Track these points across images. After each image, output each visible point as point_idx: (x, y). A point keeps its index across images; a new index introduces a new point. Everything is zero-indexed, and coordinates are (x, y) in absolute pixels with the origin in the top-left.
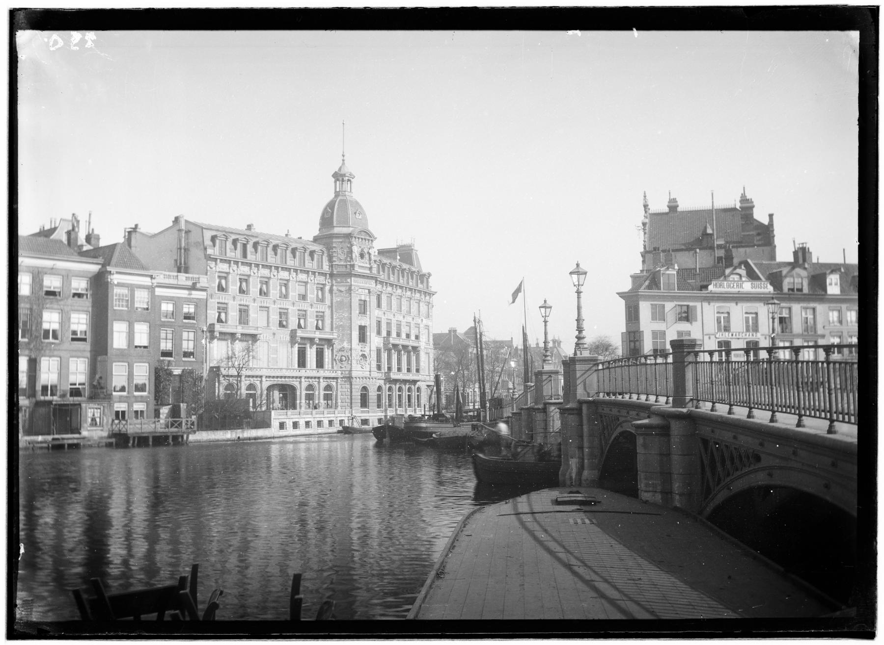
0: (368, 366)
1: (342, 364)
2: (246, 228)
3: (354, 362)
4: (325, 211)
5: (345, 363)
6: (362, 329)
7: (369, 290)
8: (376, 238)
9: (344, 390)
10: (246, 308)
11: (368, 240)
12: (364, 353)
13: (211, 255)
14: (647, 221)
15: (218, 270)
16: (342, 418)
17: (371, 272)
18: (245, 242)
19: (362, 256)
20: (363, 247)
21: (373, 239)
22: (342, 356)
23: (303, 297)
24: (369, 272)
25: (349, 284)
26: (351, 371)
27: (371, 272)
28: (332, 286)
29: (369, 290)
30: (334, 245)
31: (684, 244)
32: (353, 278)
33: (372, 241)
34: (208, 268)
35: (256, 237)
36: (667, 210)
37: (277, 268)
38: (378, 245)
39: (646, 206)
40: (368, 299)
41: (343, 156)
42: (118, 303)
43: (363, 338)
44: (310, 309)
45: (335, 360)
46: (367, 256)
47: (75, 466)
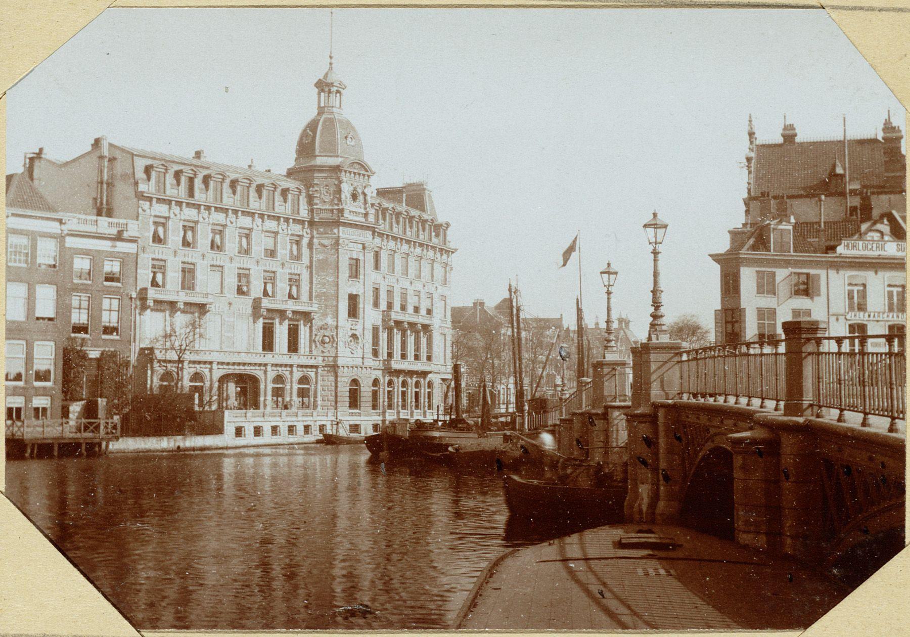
2: (194, 155)
4: (304, 135)
6: (353, 300)
7: (363, 244)
8: (374, 173)
11: (364, 175)
13: (144, 192)
18: (192, 176)
19: (354, 197)
20: (355, 185)
22: (325, 336)
23: (272, 253)
24: (363, 220)
26: (336, 357)
28: (312, 238)
29: (363, 244)
30: (316, 181)
33: (368, 176)
35: (367, 171)
36: (781, 140)
38: (377, 182)
39: (751, 134)
41: (331, 57)
43: (353, 312)
44: (229, 265)
46: (361, 198)
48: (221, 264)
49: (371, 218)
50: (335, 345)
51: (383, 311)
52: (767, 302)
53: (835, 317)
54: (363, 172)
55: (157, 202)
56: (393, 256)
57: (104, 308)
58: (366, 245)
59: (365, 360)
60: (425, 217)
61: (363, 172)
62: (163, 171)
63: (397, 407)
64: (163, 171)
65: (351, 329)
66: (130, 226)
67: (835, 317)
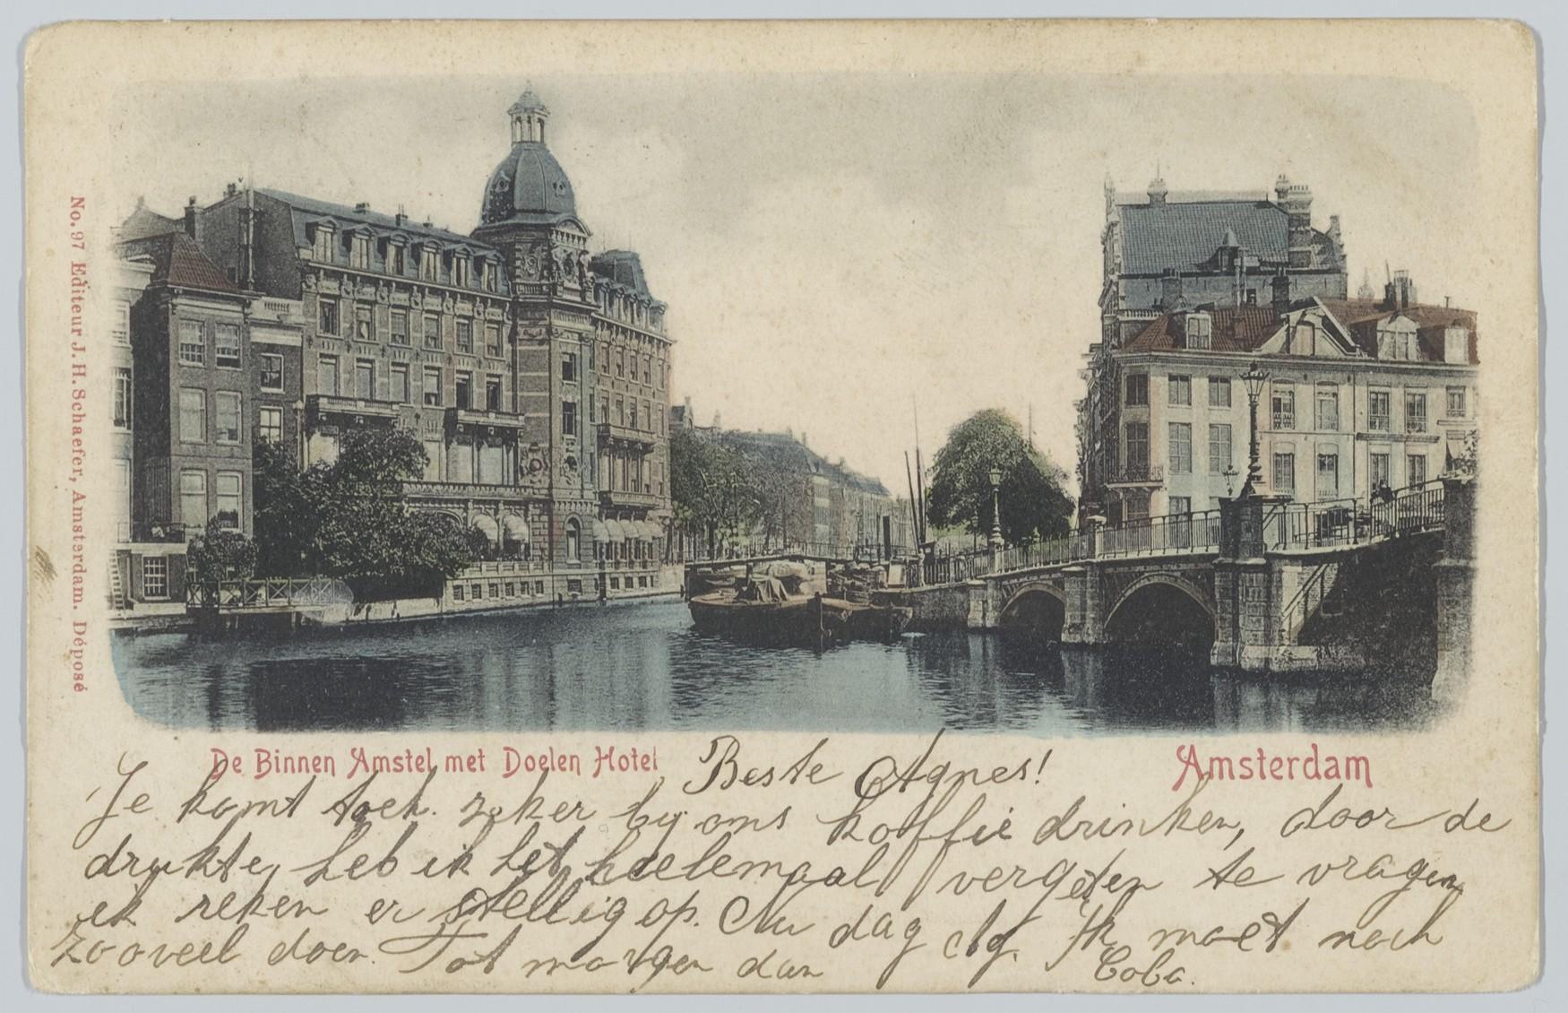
0: (578, 480)
1: (534, 476)
3: (556, 471)
5: (539, 474)
6: (569, 407)
7: (580, 334)
9: (537, 525)
10: (496, 380)
11: (579, 238)
12: (571, 454)
13: (309, 261)
14: (1114, 218)
15: (392, 303)
16: (478, 582)
17: (584, 299)
18: (401, 244)
20: (569, 251)
21: (585, 235)
24: (579, 299)
25: (547, 322)
26: (550, 488)
27: (584, 299)
28: (514, 327)
29: (580, 334)
31: (1198, 266)
32: (553, 311)
33: (585, 240)
34: (304, 285)
35: (581, 230)
37: (388, 284)
40: (577, 353)
42: (185, 352)
43: (569, 426)
44: (477, 369)
45: (521, 468)
46: (576, 270)
47: (1053, 609)
48: (335, 353)
49: (590, 297)
50: (547, 473)
51: (599, 425)
52: (1220, 415)
53: (66, 959)
54: (577, 233)
55: (430, 293)
56: (469, 328)
57: (262, 424)
58: (584, 335)
59: (585, 492)
60: (631, 291)
61: (577, 233)
62: (331, 230)
63: (601, 556)
64: (331, 230)
65: (567, 450)
66: (292, 310)
67: (67, 958)
